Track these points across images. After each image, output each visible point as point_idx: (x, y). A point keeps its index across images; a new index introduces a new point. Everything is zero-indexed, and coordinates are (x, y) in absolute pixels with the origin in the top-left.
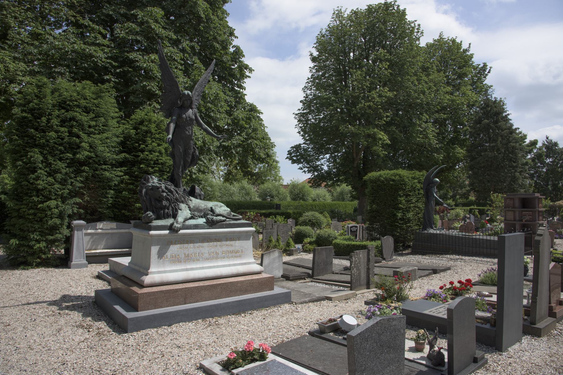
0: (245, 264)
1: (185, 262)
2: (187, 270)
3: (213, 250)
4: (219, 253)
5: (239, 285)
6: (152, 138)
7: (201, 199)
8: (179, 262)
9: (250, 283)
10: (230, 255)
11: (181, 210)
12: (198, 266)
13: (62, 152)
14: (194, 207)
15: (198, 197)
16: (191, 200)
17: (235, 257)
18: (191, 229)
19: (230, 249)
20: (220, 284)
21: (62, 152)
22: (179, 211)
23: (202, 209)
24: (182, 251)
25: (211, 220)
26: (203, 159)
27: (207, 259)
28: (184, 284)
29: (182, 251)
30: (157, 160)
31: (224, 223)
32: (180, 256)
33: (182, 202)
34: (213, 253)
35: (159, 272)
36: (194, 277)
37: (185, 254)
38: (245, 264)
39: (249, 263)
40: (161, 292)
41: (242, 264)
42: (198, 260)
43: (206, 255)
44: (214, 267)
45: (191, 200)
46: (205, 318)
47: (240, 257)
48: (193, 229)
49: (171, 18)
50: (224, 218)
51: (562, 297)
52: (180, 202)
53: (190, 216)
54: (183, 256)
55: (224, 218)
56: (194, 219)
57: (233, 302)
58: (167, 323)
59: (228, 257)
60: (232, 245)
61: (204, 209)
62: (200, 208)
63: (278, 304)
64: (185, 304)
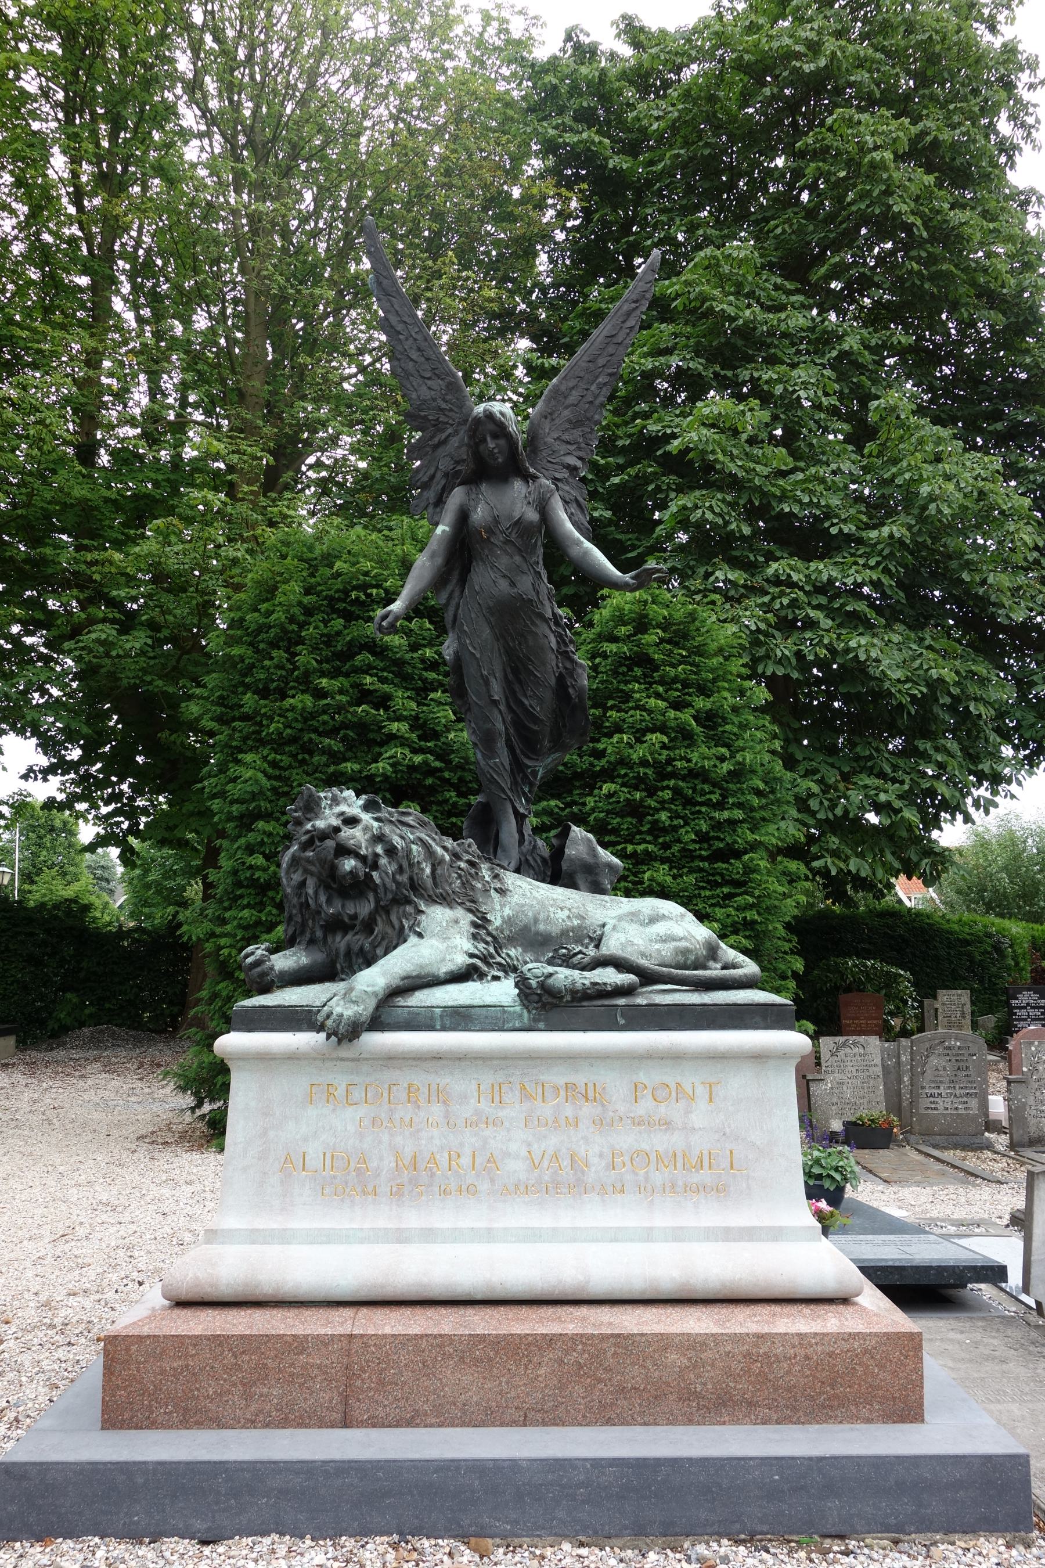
0: (749, 1234)
1: (397, 1193)
2: (401, 1237)
3: (553, 1141)
4: (594, 1160)
5: (673, 1357)
6: (651, 684)
7: (597, 889)
8: (364, 1193)
9: (748, 1355)
10: (658, 1178)
11: (420, 935)
12: (466, 1222)
13: (336, 758)
14: (508, 921)
15: (580, 880)
16: (502, 892)
17: (686, 1188)
18: (431, 1028)
19: (659, 1142)
20: (551, 1340)
21: (336, 758)
22: (413, 939)
23: (555, 930)
24: (385, 1138)
25: (542, 985)
26: (931, 752)
27: (519, 1189)
28: (364, 1311)
29: (385, 1138)
30: (670, 761)
31: (622, 1001)
32: (373, 1164)
33: (445, 900)
34: (556, 1157)
35: (254, 1236)
36: (425, 1280)
37: (397, 1155)
38: (749, 1234)
39: (776, 1234)
40: (219, 1341)
41: (728, 1235)
42: (471, 1190)
43: (516, 1168)
44: (555, 1235)
45: (502, 892)
46: (419, 1532)
47: (719, 1191)
48: (444, 1029)
49: (833, 286)
50: (627, 978)
51: (1031, 225)
52: (432, 900)
53: (460, 960)
54: (389, 1162)
55: (627, 978)
56: (482, 976)
57: (598, 1464)
58: (199, 1525)
59: (646, 1190)
60: (666, 1125)
61: (564, 933)
62: (542, 927)
63: (925, 1525)
64: (346, 1422)
